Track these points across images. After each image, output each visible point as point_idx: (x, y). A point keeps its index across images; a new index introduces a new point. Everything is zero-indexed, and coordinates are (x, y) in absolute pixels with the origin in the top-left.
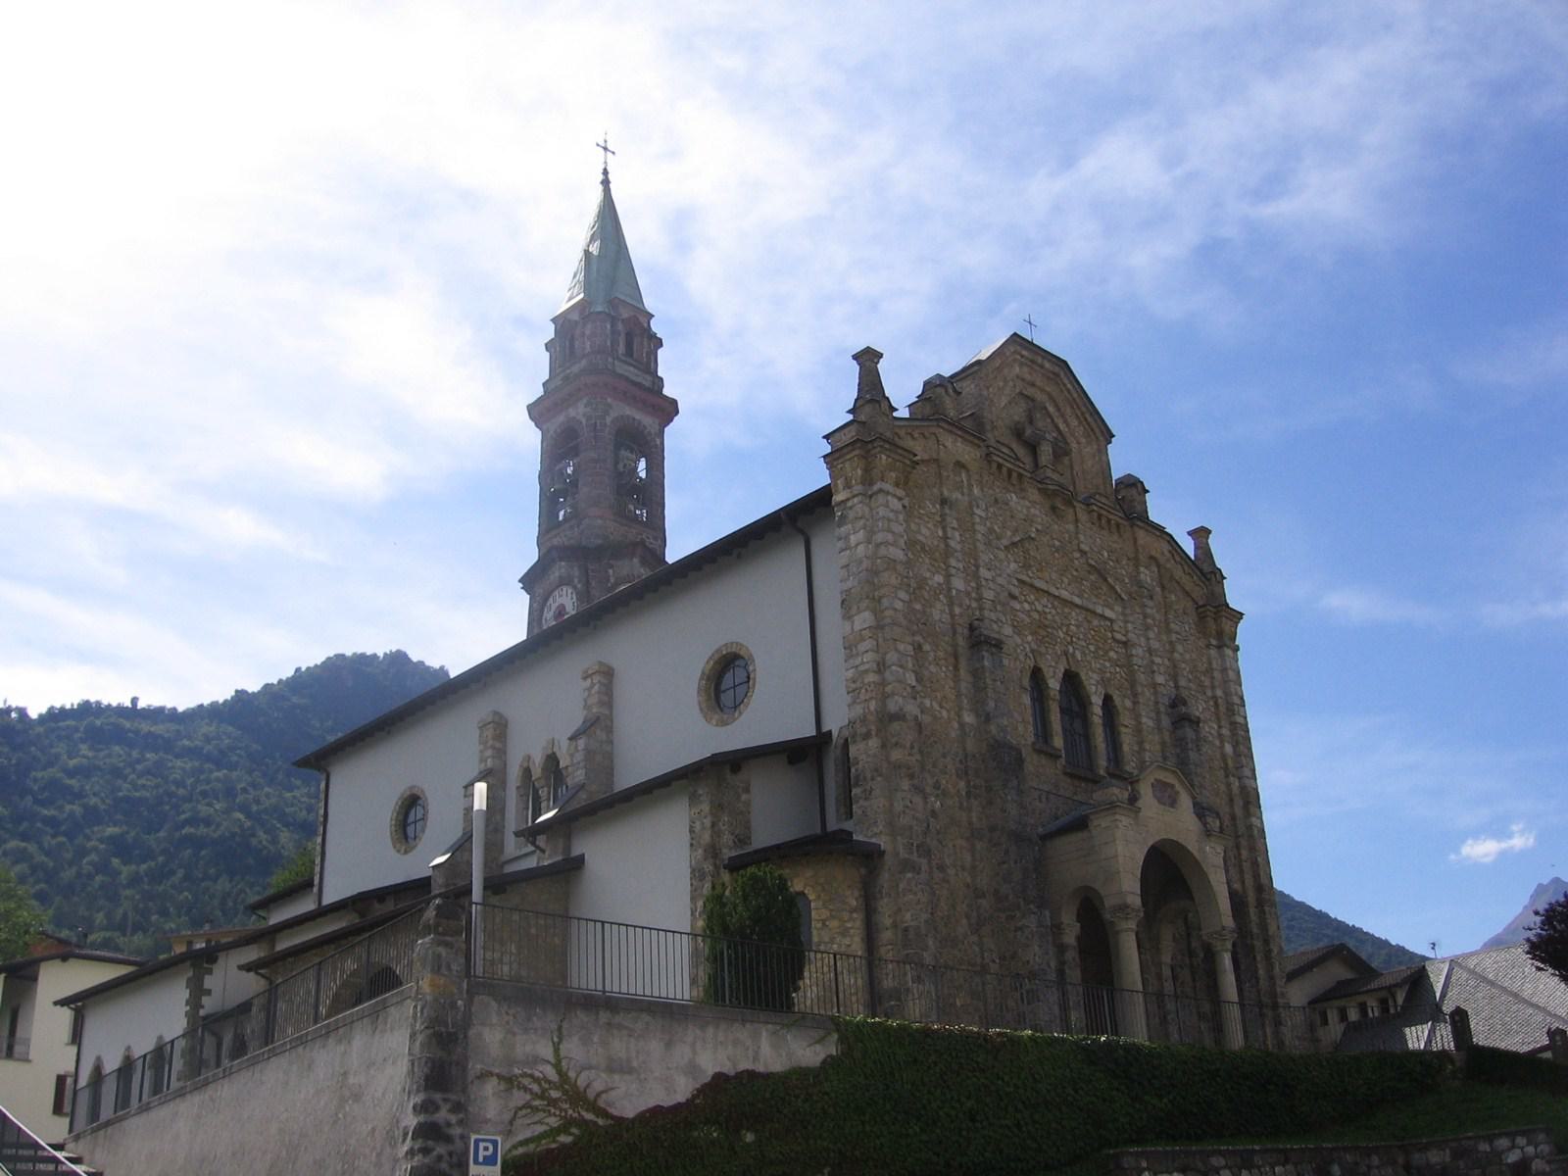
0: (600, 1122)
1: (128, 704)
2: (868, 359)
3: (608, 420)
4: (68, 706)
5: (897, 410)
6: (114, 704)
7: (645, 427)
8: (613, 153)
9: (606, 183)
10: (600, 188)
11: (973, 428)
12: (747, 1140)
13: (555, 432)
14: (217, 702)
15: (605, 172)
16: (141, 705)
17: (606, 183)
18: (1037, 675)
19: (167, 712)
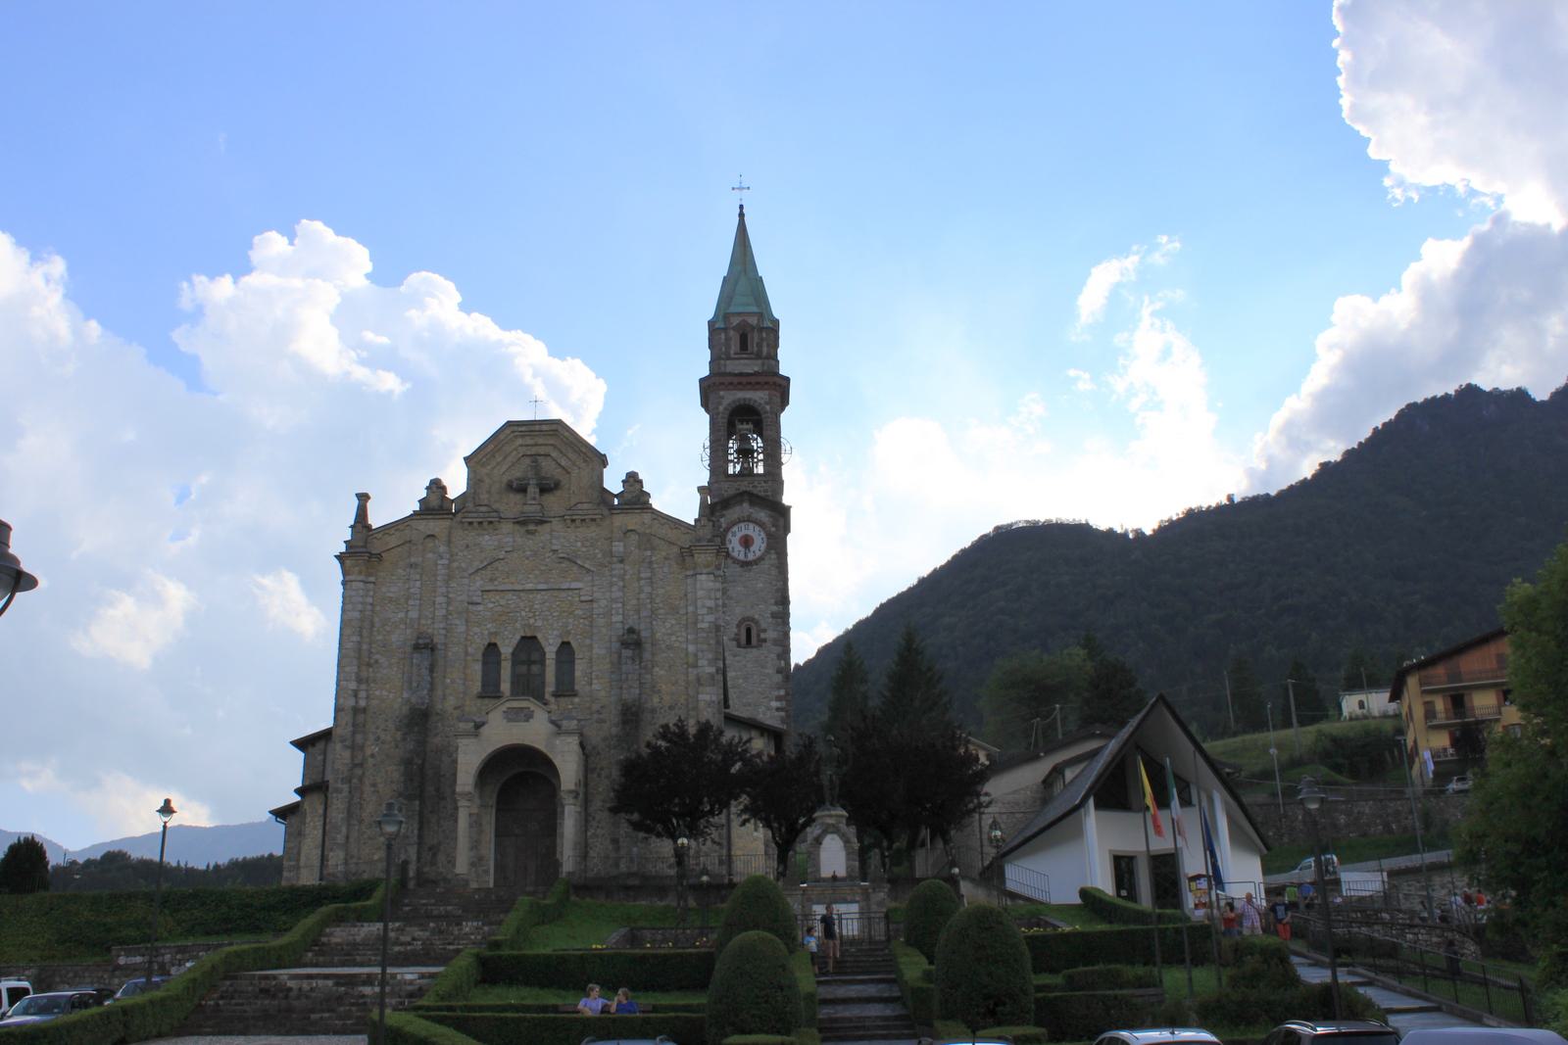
0: (1213, 883)
1: (1225, 501)
2: (363, 498)
3: (721, 408)
4: (1175, 518)
5: (437, 487)
6: (1214, 505)
7: (755, 401)
8: (733, 189)
9: (741, 215)
10: (738, 219)
11: (720, 358)
12: (121, 958)
13: (1127, 257)
14: (1306, 479)
15: (741, 207)
16: (1237, 500)
17: (741, 215)
18: (492, 649)
19: (1131, 536)
